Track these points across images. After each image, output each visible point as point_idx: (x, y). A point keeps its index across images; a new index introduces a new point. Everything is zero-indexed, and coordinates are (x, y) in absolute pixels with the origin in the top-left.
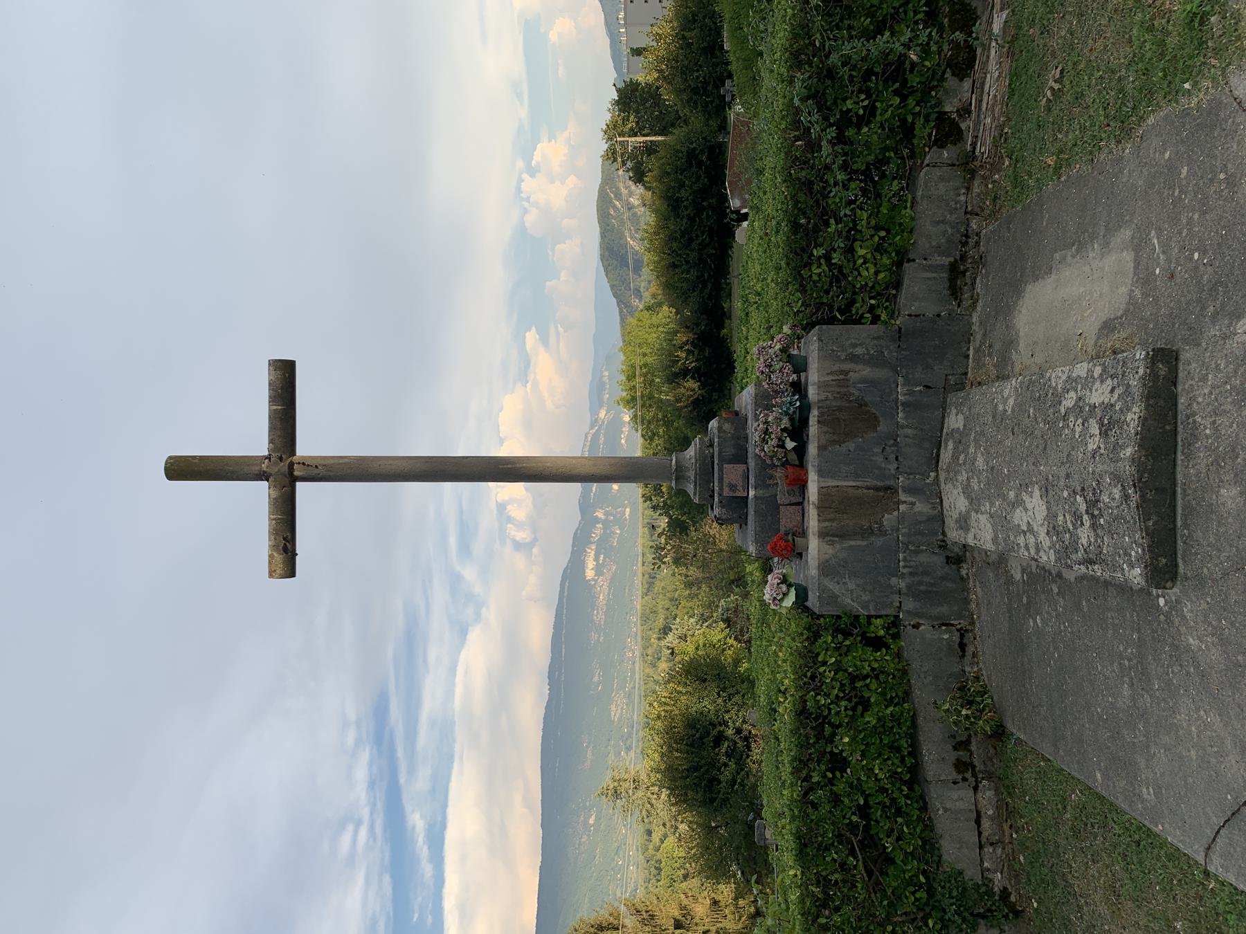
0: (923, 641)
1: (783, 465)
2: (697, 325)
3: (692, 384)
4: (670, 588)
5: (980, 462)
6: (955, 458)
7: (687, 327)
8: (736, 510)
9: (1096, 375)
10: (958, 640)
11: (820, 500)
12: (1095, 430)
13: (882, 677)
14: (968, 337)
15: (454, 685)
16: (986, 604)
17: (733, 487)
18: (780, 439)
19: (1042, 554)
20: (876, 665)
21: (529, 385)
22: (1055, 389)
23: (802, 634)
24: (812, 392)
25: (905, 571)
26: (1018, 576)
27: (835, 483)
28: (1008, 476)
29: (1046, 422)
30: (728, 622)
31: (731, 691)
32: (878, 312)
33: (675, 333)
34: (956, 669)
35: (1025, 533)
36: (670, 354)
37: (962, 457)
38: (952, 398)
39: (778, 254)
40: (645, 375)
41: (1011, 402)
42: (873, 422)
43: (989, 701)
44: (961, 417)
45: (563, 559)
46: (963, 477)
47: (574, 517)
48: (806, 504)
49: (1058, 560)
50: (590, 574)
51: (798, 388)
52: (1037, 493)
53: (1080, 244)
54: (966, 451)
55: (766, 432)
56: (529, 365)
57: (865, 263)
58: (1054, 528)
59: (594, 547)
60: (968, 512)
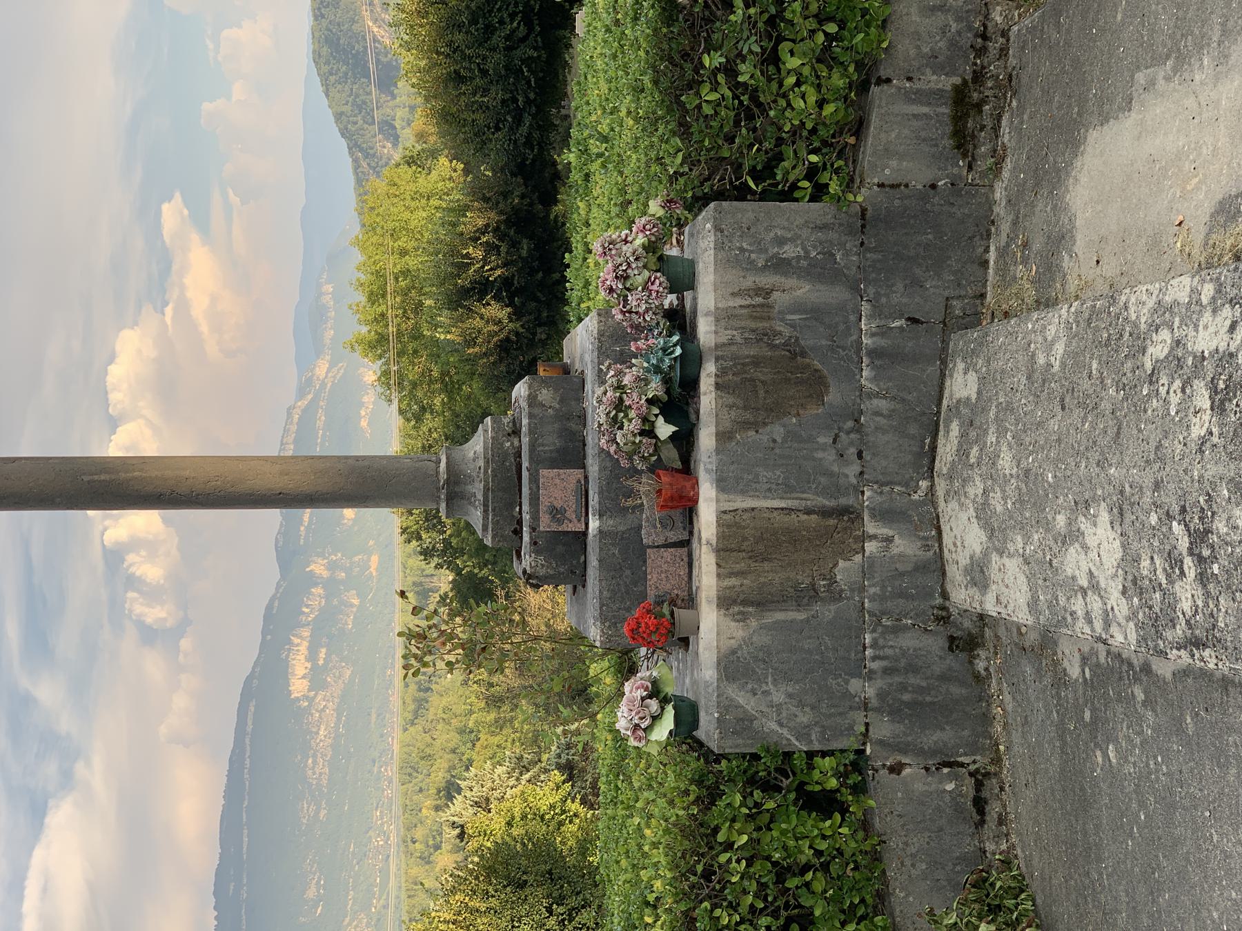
0: (908, 796)
1: (652, 469)
2: (505, 195)
3: (497, 310)
4: (461, 708)
5: (1006, 462)
6: (963, 452)
7: (486, 200)
8: (565, 557)
9: (1205, 301)
10: (972, 793)
11: (721, 537)
12: (1203, 400)
13: (835, 869)
14: (985, 226)
15: (19, 917)
16: (1021, 722)
17: (557, 514)
18: (645, 420)
19: (1114, 630)
20: (823, 846)
21: (169, 311)
22: (1136, 325)
23: (687, 792)
24: (705, 331)
25: (875, 665)
26: (1074, 671)
27: (749, 503)
28: (1055, 487)
29: (1121, 387)
30: (570, 770)
31: (573, 902)
32: (824, 178)
33: (462, 210)
34: (969, 846)
35: (1084, 591)
36: (454, 252)
37: (975, 451)
38: (958, 341)
39: (638, 59)
40: (405, 293)
41: (1060, 348)
42: (816, 385)
43: (1028, 905)
44: (972, 377)
45: (244, 655)
46: (976, 489)
47: (266, 578)
48: (695, 545)
49: (1142, 640)
50: (298, 686)
51: (679, 320)
52: (1104, 517)
53: (1178, 54)
54: (980, 440)
55: (619, 405)
56: (166, 270)
57: (798, 84)
58: (1134, 581)
59: (306, 633)
60: (986, 554)
